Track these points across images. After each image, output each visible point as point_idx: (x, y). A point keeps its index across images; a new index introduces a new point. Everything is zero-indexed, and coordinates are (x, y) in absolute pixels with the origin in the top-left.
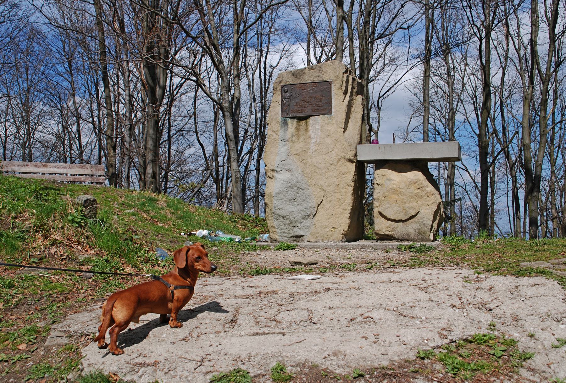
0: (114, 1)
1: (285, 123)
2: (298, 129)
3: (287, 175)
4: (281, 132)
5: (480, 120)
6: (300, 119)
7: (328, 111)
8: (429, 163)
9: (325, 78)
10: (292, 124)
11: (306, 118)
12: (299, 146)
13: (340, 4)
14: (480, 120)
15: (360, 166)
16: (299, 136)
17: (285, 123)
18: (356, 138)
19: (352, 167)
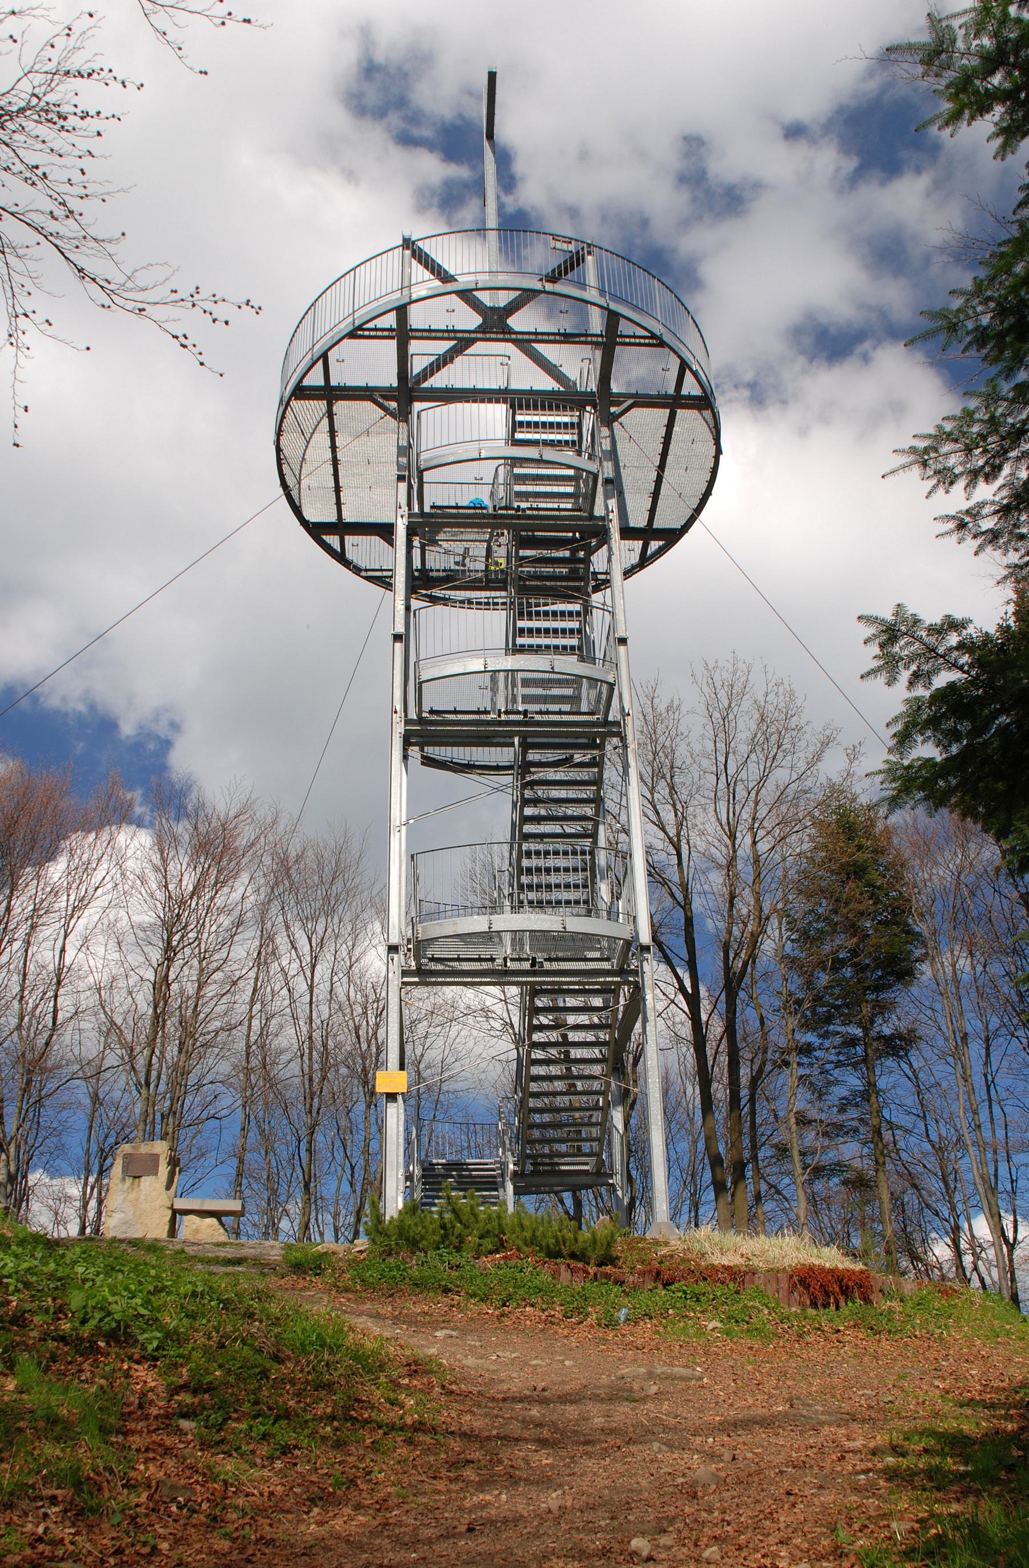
0: (2, 112)
1: (124, 1179)
2: (132, 1184)
3: (123, 1215)
4: (120, 1185)
5: (416, 979)
6: (135, 1177)
7: (156, 1174)
8: (641, 542)
9: (155, 1151)
10: (129, 1181)
11: (139, 1177)
12: (132, 1196)
13: (2, 1536)
14: (416, 979)
15: (175, 1213)
16: (133, 1189)
17: (124, 1179)
18: (173, 1195)
19: (170, 1212)
